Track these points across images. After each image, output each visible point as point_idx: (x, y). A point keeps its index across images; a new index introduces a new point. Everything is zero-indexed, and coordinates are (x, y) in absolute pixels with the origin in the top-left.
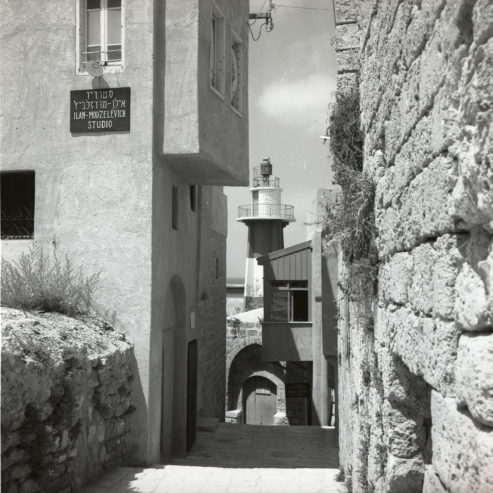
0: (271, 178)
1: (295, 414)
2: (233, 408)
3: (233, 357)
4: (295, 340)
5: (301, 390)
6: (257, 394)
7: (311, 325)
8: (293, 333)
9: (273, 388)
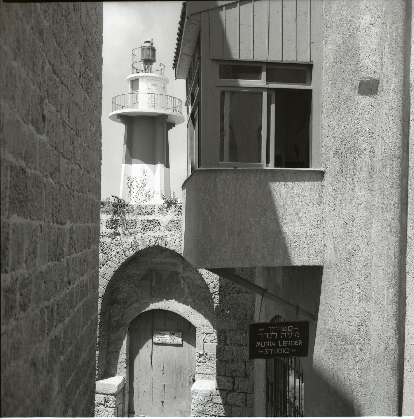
0: (155, 66)
1: (234, 383)
2: (108, 373)
3: (110, 274)
4: (280, 212)
5: (288, 339)
6: (156, 344)
7: (320, 175)
8: (276, 195)
9: (187, 331)
